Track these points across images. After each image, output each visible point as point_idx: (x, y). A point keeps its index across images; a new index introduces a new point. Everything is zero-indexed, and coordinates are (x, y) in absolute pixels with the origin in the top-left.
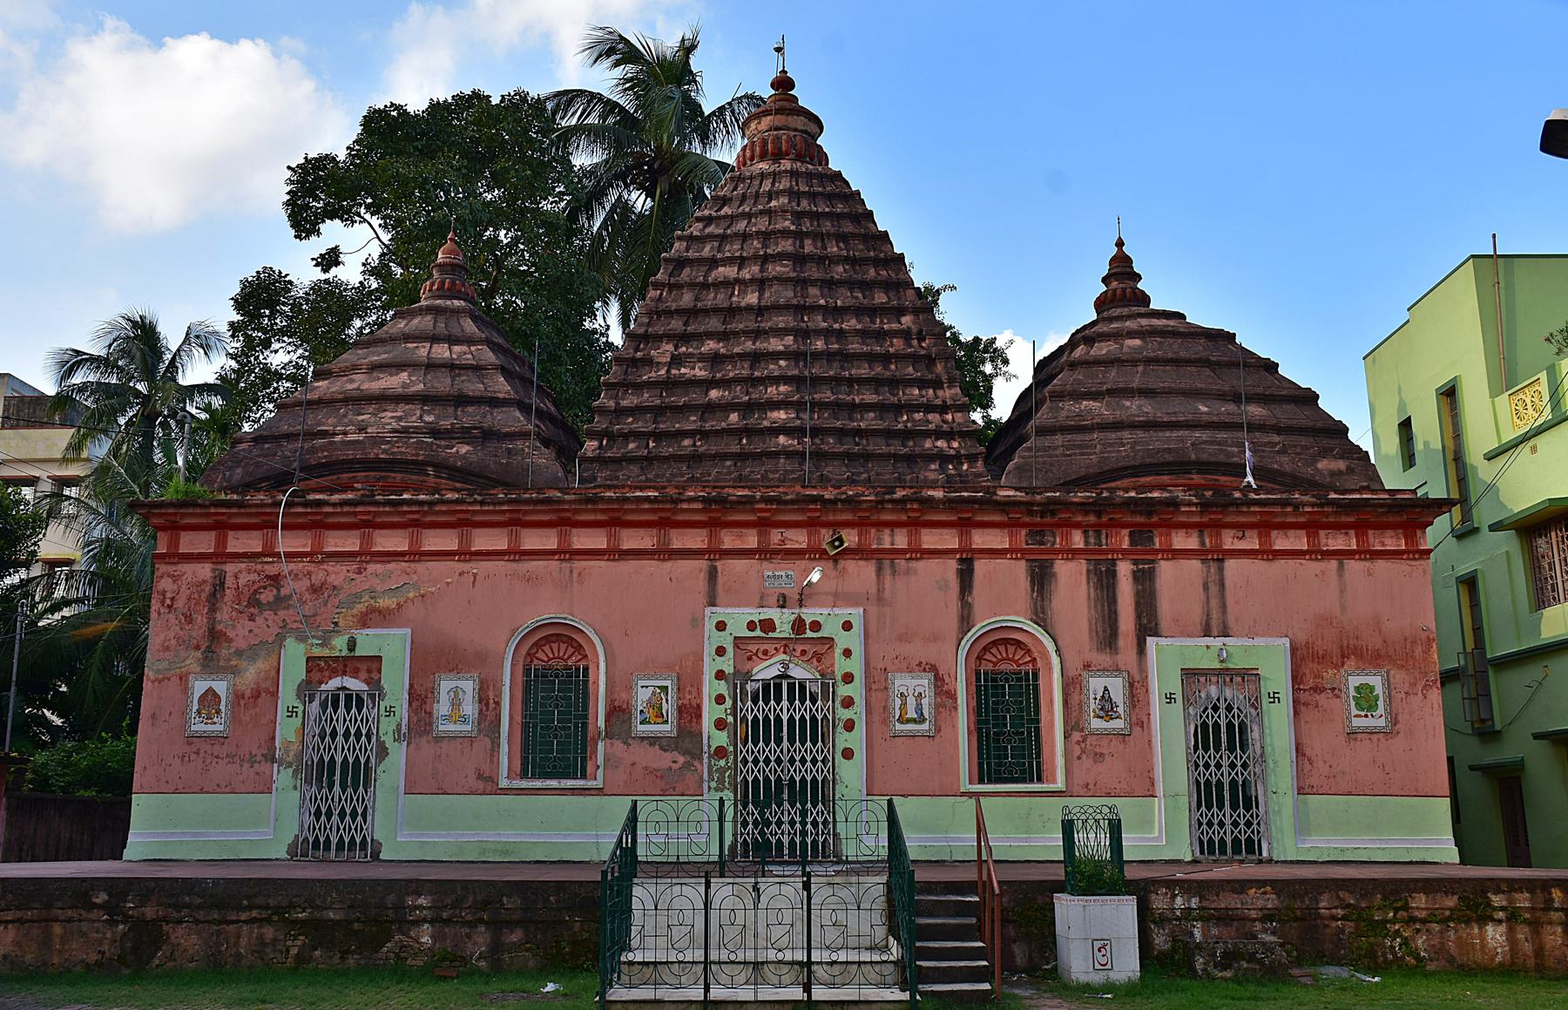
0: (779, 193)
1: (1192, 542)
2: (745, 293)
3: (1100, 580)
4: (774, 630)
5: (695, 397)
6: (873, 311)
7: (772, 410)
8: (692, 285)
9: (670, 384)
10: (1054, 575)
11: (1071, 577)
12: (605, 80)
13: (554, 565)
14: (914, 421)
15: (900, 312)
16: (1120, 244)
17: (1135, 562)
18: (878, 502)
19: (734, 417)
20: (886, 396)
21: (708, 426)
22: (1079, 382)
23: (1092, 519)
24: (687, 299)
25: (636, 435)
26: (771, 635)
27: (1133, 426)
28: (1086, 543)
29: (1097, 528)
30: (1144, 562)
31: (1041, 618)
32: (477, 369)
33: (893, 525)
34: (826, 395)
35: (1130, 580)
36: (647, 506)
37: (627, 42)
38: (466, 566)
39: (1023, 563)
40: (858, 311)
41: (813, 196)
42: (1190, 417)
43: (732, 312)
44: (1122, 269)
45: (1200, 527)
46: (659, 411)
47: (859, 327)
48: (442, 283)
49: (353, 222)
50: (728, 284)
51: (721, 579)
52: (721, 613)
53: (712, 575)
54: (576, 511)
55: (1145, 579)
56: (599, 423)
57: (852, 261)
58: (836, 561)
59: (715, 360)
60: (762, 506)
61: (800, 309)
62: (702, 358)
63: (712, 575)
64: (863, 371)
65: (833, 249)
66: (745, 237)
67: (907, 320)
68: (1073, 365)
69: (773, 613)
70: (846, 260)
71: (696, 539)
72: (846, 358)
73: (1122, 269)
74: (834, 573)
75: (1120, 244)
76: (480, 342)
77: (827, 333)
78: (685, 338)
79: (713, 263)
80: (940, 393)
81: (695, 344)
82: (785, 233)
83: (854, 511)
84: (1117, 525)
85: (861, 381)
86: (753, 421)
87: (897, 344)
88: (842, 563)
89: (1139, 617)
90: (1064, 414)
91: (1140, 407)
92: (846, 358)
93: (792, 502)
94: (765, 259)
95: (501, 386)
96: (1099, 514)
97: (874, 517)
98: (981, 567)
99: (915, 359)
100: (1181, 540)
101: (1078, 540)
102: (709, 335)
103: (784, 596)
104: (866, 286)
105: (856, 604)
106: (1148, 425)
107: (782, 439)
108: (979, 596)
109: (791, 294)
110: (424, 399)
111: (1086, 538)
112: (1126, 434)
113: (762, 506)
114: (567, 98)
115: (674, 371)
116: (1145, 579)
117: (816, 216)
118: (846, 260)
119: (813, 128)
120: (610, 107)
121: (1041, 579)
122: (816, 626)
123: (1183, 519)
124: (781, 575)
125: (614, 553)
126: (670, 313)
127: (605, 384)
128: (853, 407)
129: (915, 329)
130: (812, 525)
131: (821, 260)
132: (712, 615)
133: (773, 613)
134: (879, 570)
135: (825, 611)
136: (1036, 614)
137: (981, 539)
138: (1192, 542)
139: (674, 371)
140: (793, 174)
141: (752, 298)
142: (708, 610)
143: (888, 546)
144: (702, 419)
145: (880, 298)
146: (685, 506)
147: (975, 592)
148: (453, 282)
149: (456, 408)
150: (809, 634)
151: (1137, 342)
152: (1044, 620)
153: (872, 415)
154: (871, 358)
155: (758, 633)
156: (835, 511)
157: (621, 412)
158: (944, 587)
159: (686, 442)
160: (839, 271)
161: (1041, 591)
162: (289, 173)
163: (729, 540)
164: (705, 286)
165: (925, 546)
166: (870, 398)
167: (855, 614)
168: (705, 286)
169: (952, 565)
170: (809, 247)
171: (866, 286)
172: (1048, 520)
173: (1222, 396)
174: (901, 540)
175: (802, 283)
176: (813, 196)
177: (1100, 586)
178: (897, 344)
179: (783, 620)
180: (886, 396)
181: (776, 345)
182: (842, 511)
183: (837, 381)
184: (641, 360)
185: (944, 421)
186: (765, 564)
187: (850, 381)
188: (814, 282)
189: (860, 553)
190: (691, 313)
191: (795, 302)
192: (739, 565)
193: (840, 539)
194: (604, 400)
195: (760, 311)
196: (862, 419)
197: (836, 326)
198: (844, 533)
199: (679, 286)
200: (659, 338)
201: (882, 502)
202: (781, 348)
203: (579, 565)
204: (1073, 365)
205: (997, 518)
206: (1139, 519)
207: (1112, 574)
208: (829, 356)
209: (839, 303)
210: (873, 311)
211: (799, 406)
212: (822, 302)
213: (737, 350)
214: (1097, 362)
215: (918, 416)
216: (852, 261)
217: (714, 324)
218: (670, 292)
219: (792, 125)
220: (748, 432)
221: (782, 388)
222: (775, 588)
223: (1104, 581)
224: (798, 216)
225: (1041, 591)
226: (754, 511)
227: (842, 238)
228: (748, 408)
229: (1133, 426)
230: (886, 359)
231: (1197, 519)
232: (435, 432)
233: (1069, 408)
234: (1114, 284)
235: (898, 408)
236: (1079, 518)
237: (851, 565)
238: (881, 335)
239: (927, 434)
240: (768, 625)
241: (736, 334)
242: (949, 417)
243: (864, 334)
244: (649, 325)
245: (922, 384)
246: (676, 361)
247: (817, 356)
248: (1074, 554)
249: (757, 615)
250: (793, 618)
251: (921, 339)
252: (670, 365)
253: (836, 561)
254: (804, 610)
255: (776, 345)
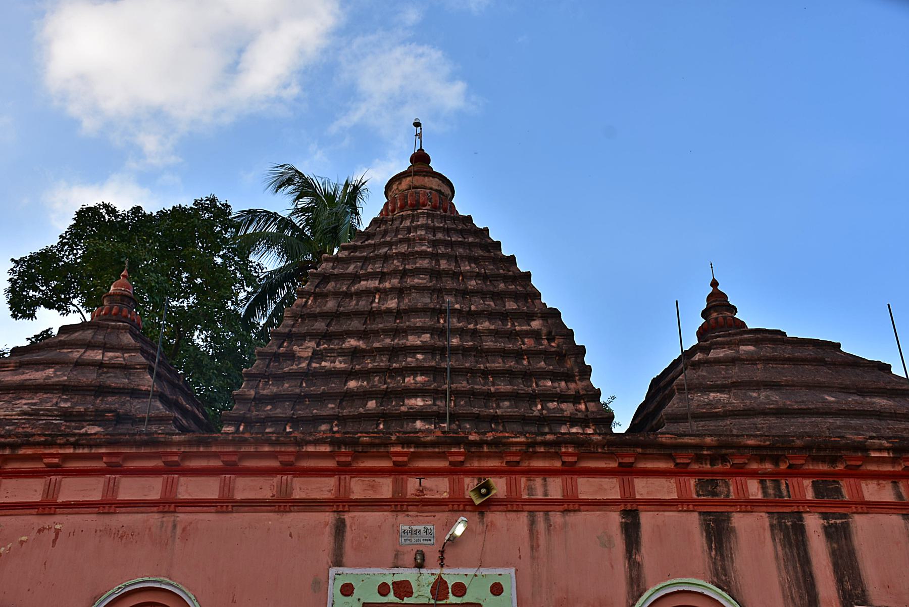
0: (416, 228)
1: (886, 494)
2: (386, 300)
3: (787, 536)
4: (410, 594)
5: (334, 386)
6: (504, 316)
7: (410, 397)
8: (336, 294)
9: (308, 375)
10: (733, 530)
11: (752, 531)
12: (283, 204)
13: (154, 518)
14: (548, 409)
15: (529, 317)
16: (714, 284)
17: (825, 516)
18: (528, 445)
19: (371, 404)
20: (520, 386)
21: (345, 412)
22: (704, 377)
23: (768, 466)
24: (331, 304)
25: (275, 420)
26: (406, 600)
27: (764, 413)
28: (765, 493)
29: (776, 476)
30: (834, 516)
31: (724, 584)
32: (125, 368)
33: (546, 473)
34: (463, 384)
35: (823, 537)
36: (266, 449)
37: (301, 175)
38: (47, 521)
39: (696, 514)
40: (491, 315)
41: (447, 231)
42: (819, 405)
43: (373, 314)
44: (718, 304)
45: (894, 478)
46: (297, 399)
47: (492, 327)
48: (111, 309)
49: (68, 312)
50: (369, 293)
51: (349, 535)
52: (347, 574)
53: (340, 529)
54: (185, 456)
55: (839, 535)
56: (238, 409)
57: (485, 277)
58: (482, 514)
59: (355, 353)
60: (398, 449)
61: (438, 312)
62: (342, 353)
63: (340, 529)
64: (498, 364)
65: (466, 267)
66: (386, 258)
67: (536, 324)
68: (696, 365)
69: (407, 574)
70: (478, 276)
71: (324, 488)
72: (481, 353)
73: (718, 304)
74: (479, 528)
75: (714, 284)
76: (134, 350)
77: (461, 332)
78: (327, 336)
79: (356, 278)
80: (572, 386)
81: (336, 341)
82: (423, 255)
83: (499, 456)
84: (795, 472)
85: (496, 373)
86: (392, 406)
87: (529, 343)
88: (490, 517)
89: (840, 581)
90: (695, 403)
91: (767, 397)
92: (481, 353)
93: (433, 444)
94: (404, 274)
95: (147, 381)
96: (776, 460)
97: (525, 464)
98: (647, 519)
99: (546, 354)
100: (871, 491)
101: (754, 489)
102: (350, 334)
103: (422, 554)
104: (498, 296)
105: (507, 565)
106: (779, 412)
107: (419, 424)
108: (647, 554)
109: (428, 300)
110: (64, 389)
111: (764, 489)
112: (759, 421)
113: (398, 449)
114: (252, 215)
115: (314, 365)
116: (839, 535)
117: (450, 244)
118: (478, 276)
119: (445, 189)
120: (285, 223)
121: (718, 534)
122: (460, 590)
123: (873, 468)
124: (419, 529)
125: (225, 504)
126: (314, 317)
127: (247, 375)
128: (488, 396)
129: (544, 331)
130: (455, 471)
131: (455, 275)
132: (338, 577)
133: (407, 574)
134: (532, 523)
135: (471, 572)
136: (717, 574)
137: (643, 488)
138: (886, 494)
139: (314, 365)
140: (426, 227)
141: (392, 304)
142: (333, 571)
143: (540, 496)
144: (340, 406)
145: (511, 305)
146: (311, 449)
147: (643, 550)
148: (120, 310)
149: (96, 397)
150: (452, 599)
151: (751, 348)
152: (728, 583)
153: (507, 403)
154: (504, 354)
155: (391, 598)
156: (481, 456)
157: (260, 400)
158: (608, 543)
159: (324, 427)
160: (472, 284)
161: (720, 548)
162: (13, 265)
163: (358, 488)
164: (348, 295)
165: (581, 497)
166: (504, 387)
167: (507, 576)
168: (348, 295)
169: (615, 518)
170: (444, 264)
171: (498, 296)
172: (719, 467)
173: (845, 389)
174: (555, 488)
175: (439, 292)
176: (447, 231)
177: (787, 542)
178: (529, 343)
179: (422, 582)
180: (520, 386)
181: (413, 340)
182: (488, 456)
183: (472, 372)
184: (283, 355)
185: (580, 411)
186: (401, 517)
187: (485, 373)
188: (449, 292)
189: (511, 504)
190: (335, 316)
191: (432, 306)
192: (373, 518)
193: (489, 488)
194: (246, 389)
195: (399, 314)
196: (498, 407)
197: (471, 326)
198: (492, 480)
199: (325, 296)
200: (301, 338)
201: (534, 444)
202: (419, 343)
203: (183, 517)
204: (696, 365)
205: (662, 465)
206: (823, 467)
207: (800, 529)
208: (464, 351)
209: (473, 307)
210: (504, 316)
211: (437, 394)
212: (457, 306)
213: (376, 345)
214: (718, 361)
215: (552, 405)
216: (485, 277)
217: (356, 324)
218: (315, 300)
219: (428, 185)
220: (385, 417)
221: (419, 379)
222: (410, 545)
223: (793, 537)
224: (434, 243)
225: (720, 548)
226: (387, 456)
227: (472, 259)
228: (384, 396)
229: (764, 413)
230: (518, 355)
231: (888, 468)
232: (66, 415)
233: (698, 399)
234: (715, 315)
235: (532, 398)
236: (754, 466)
237: (497, 517)
238: (512, 335)
239: (562, 421)
240: (403, 589)
241: (376, 333)
242: (582, 407)
243: (496, 333)
244: (293, 326)
245: (555, 376)
246: (317, 356)
247: (455, 350)
248: (750, 505)
249: (390, 576)
250: (432, 579)
251: (550, 339)
252: (311, 359)
253: (482, 514)
254: (446, 571)
255: (413, 340)
